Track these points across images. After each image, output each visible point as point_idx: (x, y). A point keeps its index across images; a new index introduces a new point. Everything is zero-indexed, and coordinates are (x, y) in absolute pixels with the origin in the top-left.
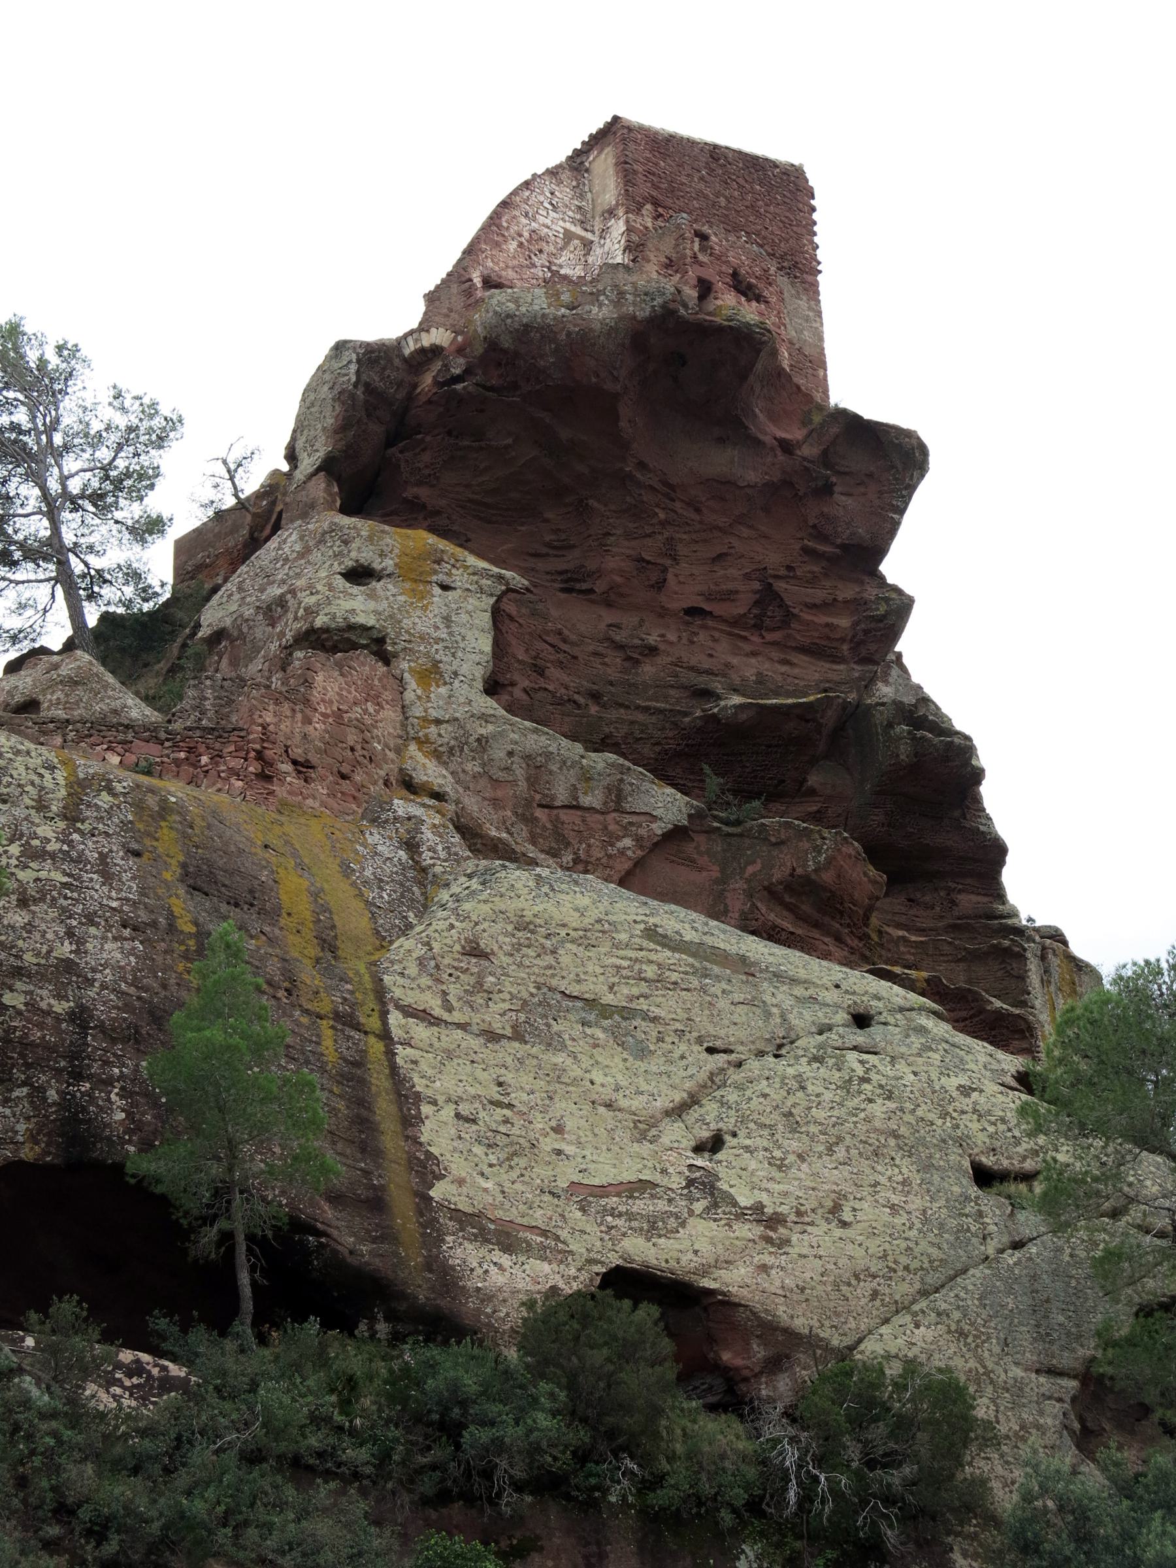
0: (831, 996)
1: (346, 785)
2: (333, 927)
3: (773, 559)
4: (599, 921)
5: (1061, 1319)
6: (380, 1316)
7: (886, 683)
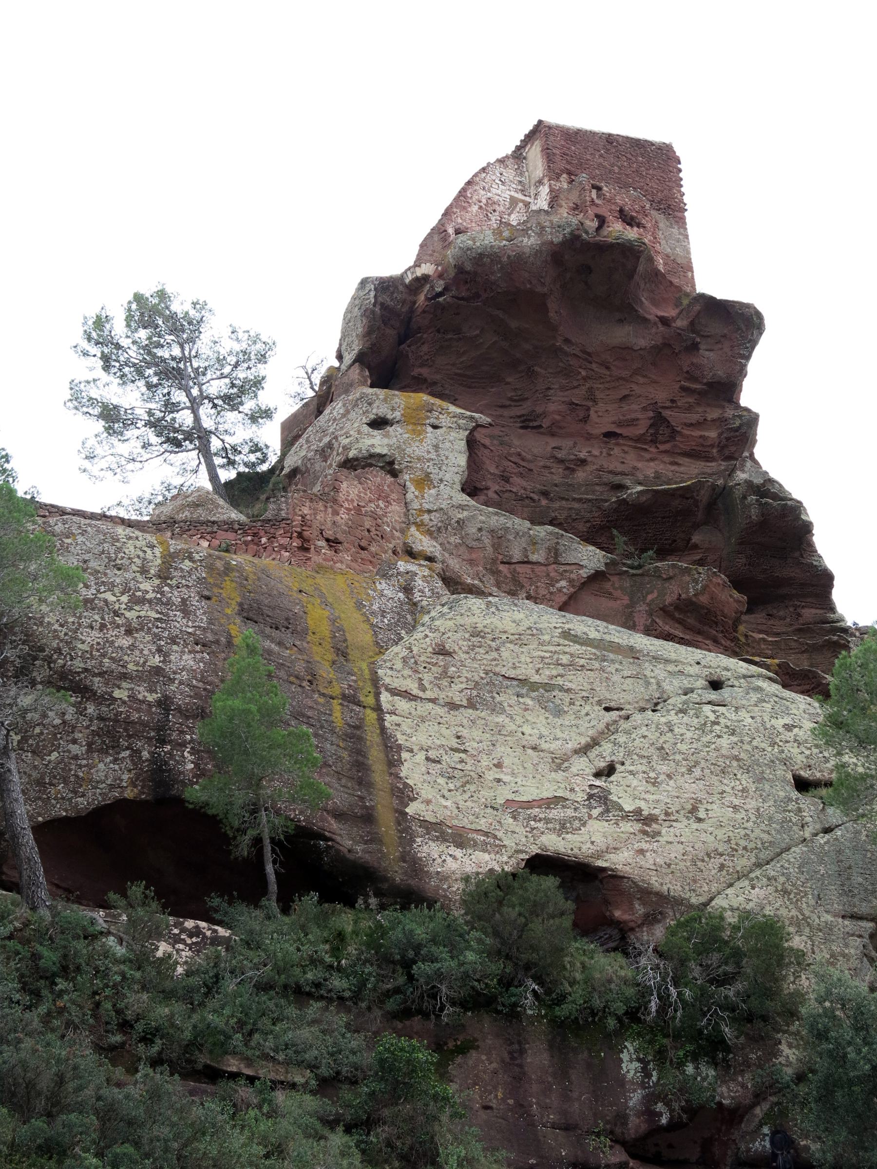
0: (694, 670)
2: (345, 640)
3: (661, 395)
4: (530, 628)
5: (860, 880)
6: (371, 893)
7: (743, 471)
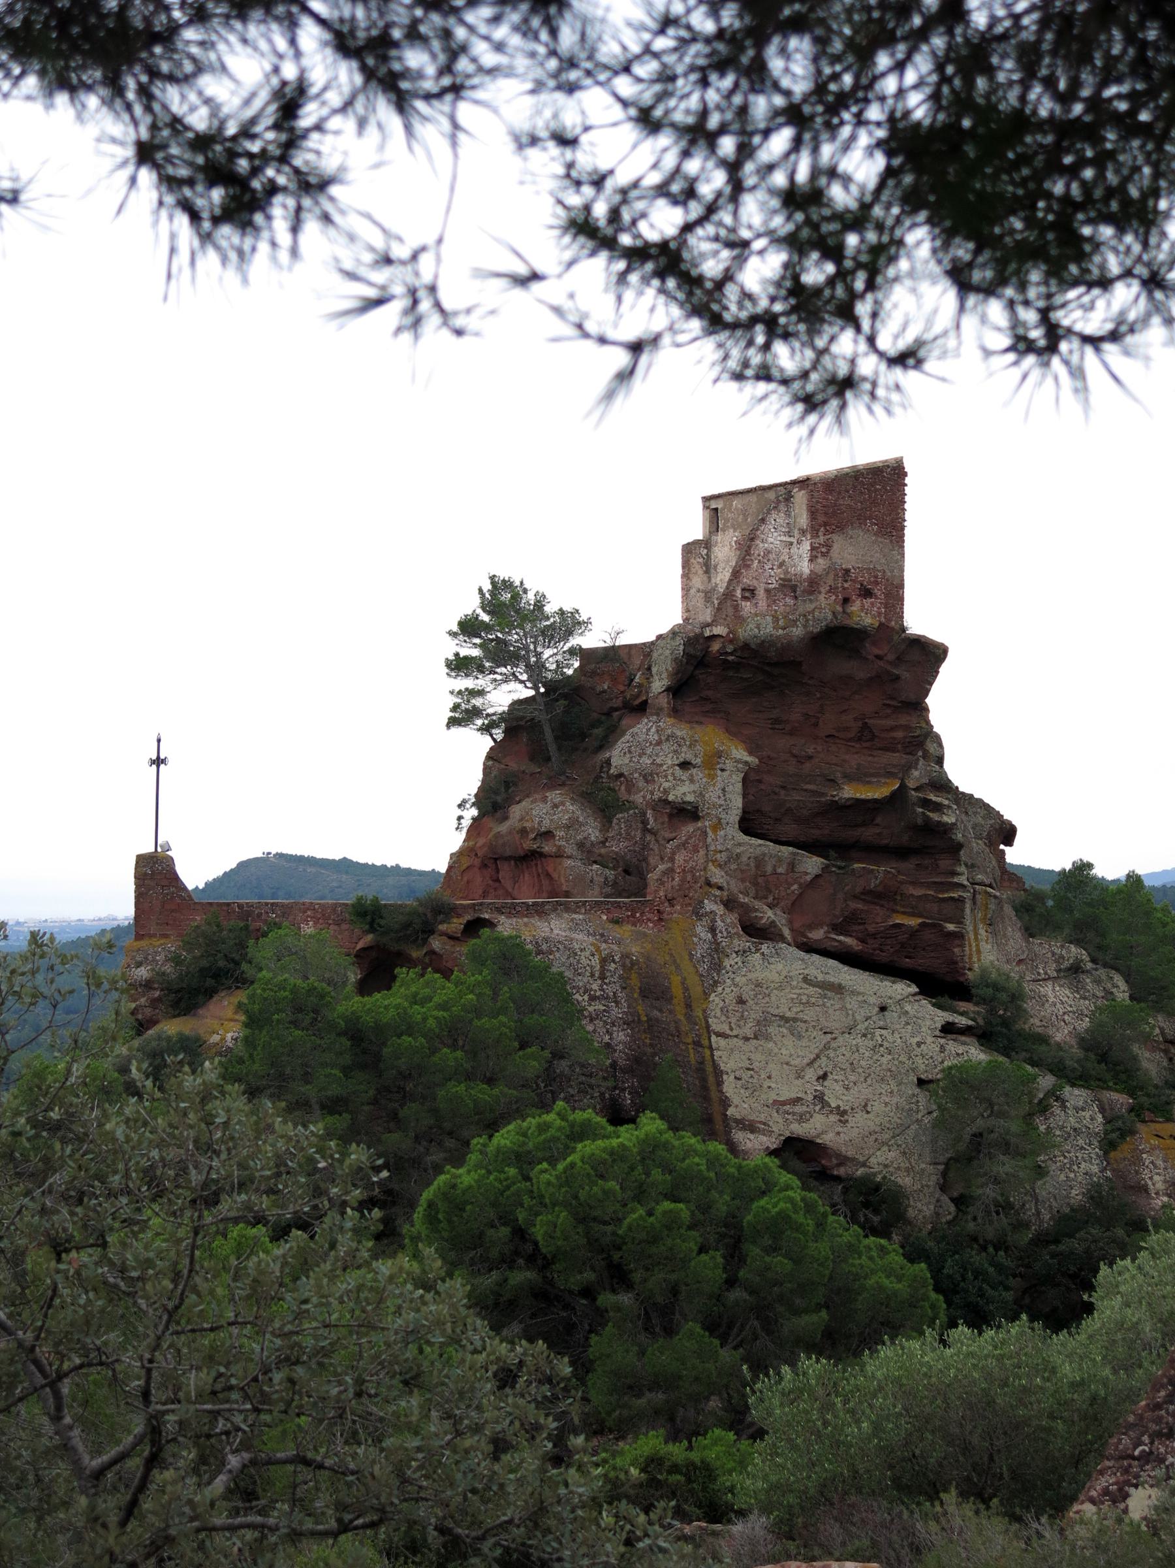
1: (687, 900)
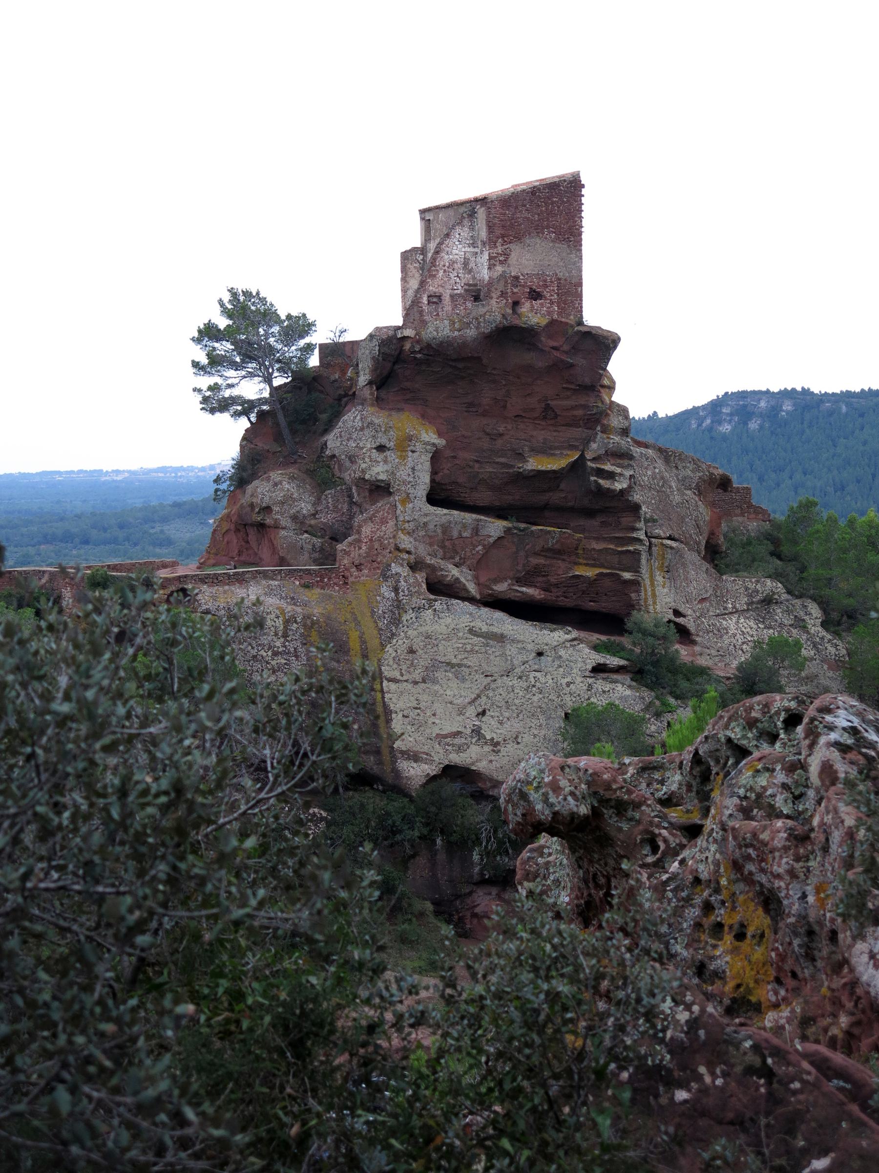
1: (375, 565)
